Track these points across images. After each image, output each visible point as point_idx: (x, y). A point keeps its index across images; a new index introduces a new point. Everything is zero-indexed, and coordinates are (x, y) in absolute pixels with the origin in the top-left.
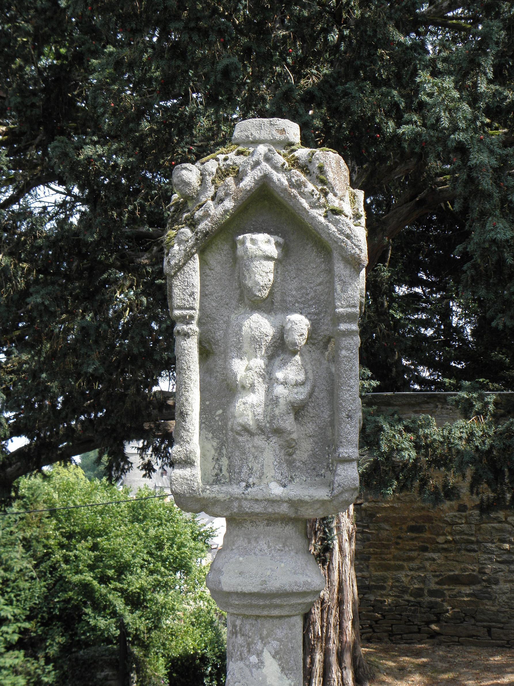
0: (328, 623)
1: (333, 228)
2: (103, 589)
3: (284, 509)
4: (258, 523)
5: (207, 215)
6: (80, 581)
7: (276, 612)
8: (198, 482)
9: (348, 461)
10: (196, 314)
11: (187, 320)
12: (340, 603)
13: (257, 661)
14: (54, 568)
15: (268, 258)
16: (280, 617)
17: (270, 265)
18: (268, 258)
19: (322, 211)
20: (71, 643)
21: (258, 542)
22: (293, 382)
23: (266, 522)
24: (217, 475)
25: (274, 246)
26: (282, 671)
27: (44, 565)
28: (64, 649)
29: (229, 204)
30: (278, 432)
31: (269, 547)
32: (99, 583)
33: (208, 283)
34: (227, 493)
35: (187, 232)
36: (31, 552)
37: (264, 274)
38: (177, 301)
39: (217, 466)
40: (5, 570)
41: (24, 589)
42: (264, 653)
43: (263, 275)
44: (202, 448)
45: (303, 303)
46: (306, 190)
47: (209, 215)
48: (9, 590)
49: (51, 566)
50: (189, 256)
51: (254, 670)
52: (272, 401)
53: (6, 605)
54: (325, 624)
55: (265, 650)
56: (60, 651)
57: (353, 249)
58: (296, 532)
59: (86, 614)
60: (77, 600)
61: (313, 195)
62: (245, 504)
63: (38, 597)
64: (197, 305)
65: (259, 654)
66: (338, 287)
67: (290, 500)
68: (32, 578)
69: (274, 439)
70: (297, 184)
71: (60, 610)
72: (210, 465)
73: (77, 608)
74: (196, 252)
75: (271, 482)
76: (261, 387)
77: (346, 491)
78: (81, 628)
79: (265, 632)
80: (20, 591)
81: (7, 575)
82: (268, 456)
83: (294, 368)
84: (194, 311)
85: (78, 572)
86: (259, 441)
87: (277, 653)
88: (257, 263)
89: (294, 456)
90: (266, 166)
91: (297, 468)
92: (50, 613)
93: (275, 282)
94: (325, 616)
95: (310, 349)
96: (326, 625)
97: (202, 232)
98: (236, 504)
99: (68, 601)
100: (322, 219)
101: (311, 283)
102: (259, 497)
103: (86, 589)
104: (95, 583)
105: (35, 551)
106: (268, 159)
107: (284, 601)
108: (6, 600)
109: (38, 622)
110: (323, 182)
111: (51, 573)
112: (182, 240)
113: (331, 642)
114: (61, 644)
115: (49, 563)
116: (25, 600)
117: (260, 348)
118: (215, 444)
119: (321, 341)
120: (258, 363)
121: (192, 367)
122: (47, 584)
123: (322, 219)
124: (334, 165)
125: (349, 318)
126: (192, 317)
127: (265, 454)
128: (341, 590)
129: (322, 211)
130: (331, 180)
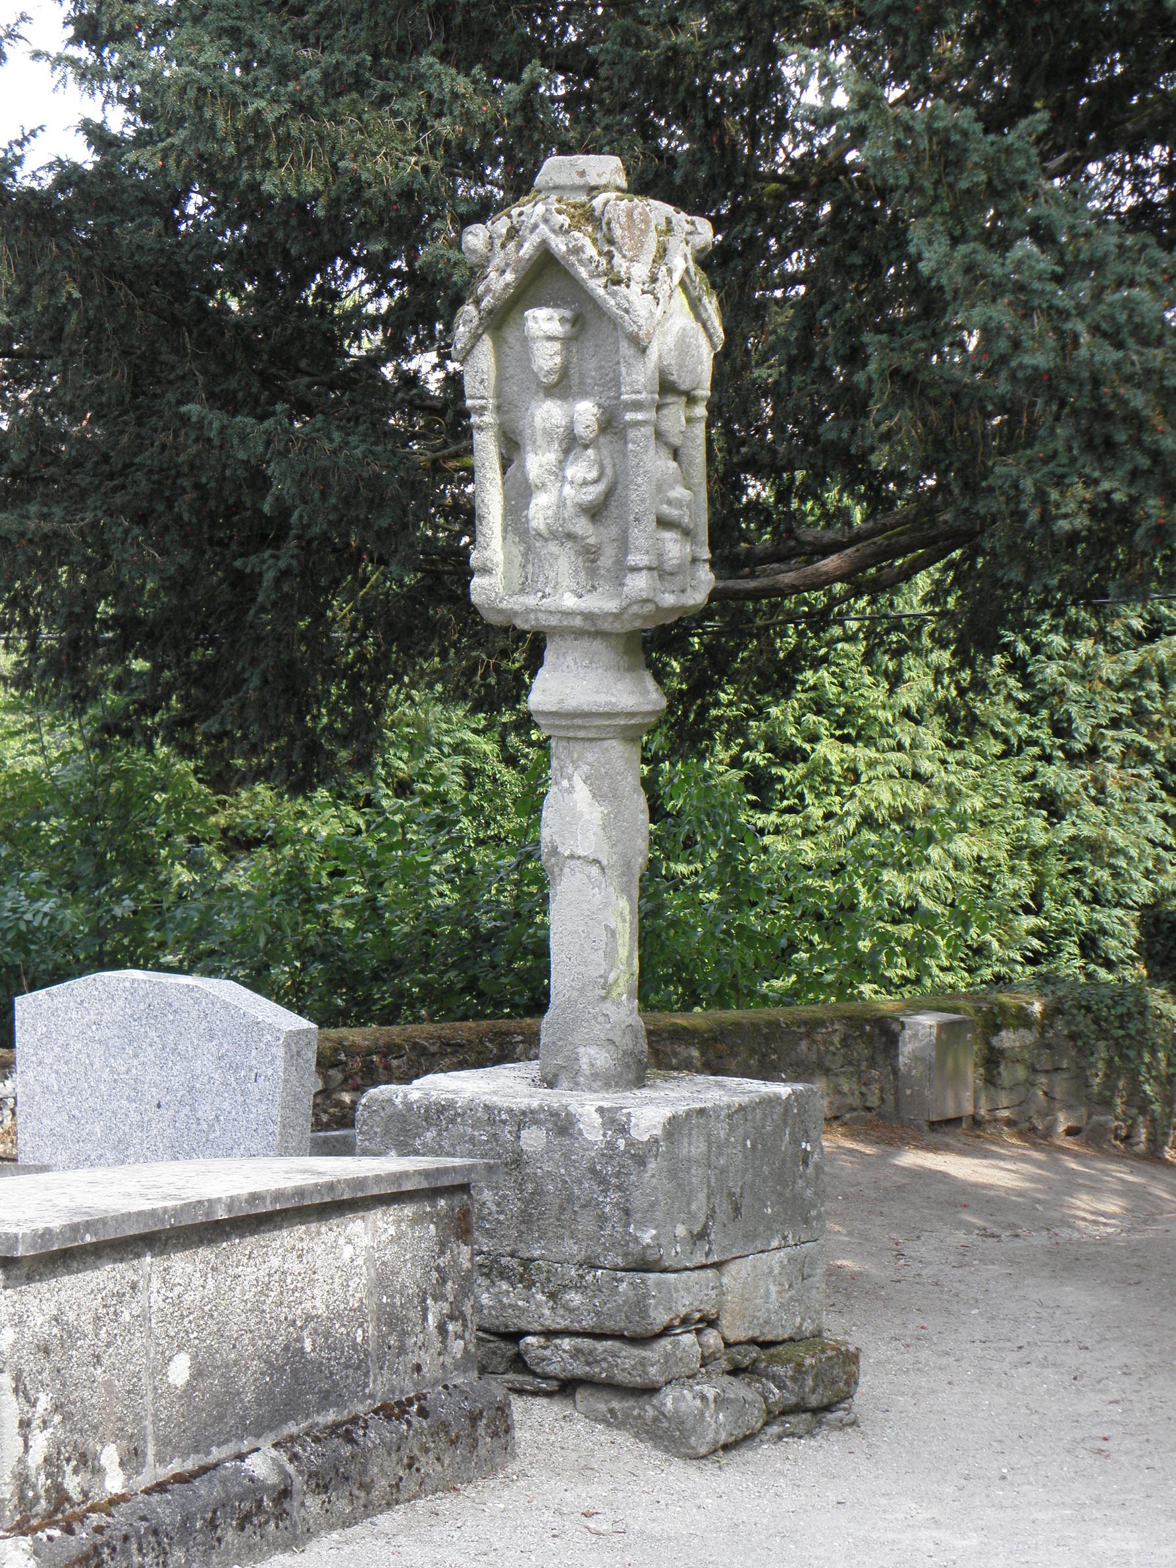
3: (578, 622)
7: (582, 734)
8: (500, 588)
9: (635, 569)
11: (481, 410)
17: (557, 346)
29: (509, 277)
30: (570, 536)
34: (523, 604)
38: (468, 391)
43: (547, 357)
45: (603, 385)
50: (476, 338)
62: (540, 615)
65: (570, 779)
69: (569, 545)
72: (517, 573)
76: (559, 486)
86: (553, 547)
87: (587, 778)
88: (538, 344)
100: (601, 291)
110: (611, 242)
120: (551, 457)
123: (601, 291)
124: (623, 220)
127: (560, 561)
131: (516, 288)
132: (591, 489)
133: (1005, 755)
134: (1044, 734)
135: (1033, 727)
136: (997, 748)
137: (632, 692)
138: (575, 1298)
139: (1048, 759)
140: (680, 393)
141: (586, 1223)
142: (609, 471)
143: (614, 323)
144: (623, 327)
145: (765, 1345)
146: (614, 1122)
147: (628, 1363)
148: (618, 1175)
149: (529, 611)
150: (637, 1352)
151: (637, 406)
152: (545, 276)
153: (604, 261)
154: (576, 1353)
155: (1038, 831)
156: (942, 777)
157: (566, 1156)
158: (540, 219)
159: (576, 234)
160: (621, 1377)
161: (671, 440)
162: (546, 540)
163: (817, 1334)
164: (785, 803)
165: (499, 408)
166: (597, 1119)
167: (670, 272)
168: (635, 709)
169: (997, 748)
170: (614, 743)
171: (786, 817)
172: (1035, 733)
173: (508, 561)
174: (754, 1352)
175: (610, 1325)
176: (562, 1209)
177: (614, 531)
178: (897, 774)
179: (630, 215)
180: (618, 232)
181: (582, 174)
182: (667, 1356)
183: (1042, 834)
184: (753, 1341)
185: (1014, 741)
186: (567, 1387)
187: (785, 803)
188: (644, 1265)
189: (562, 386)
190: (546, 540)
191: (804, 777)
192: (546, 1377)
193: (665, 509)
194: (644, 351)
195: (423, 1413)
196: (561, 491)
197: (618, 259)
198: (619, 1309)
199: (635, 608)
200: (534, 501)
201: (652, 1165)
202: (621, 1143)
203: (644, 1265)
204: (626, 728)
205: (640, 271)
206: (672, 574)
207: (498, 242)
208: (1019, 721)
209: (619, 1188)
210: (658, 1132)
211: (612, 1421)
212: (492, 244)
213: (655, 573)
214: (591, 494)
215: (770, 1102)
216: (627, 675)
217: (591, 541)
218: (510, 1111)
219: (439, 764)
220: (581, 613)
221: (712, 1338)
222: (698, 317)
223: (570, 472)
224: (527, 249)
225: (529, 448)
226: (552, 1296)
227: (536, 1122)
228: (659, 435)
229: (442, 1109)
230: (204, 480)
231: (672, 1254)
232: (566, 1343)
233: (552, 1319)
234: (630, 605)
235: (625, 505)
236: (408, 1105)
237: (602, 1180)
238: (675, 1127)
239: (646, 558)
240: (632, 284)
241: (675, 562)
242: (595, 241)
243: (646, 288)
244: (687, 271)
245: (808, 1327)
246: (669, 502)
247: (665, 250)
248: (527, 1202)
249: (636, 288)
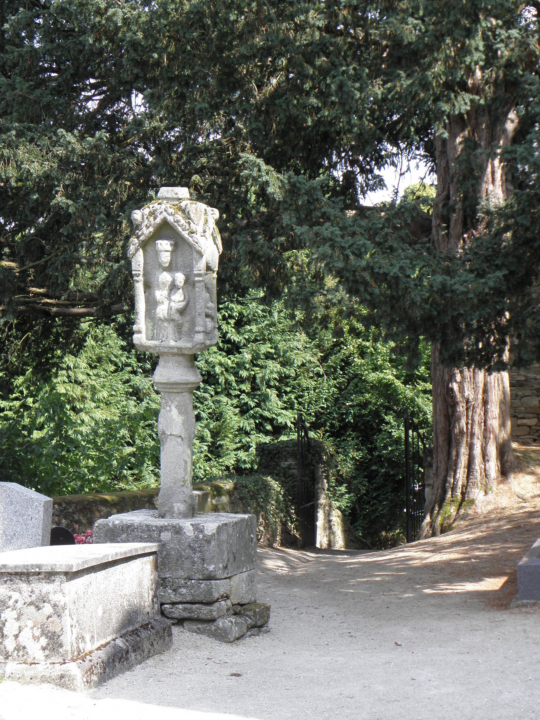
0: (473, 420)
1: (190, 239)
2: (407, 391)
3: (176, 351)
5: (143, 234)
6: (380, 381)
7: (175, 391)
9: (199, 332)
10: (141, 273)
11: (138, 275)
12: (485, 402)
14: (347, 362)
17: (169, 253)
20: (370, 460)
27: (333, 357)
28: (361, 466)
29: (151, 229)
30: (173, 320)
32: (405, 383)
35: (136, 241)
36: (316, 341)
38: (133, 268)
40: (283, 364)
41: (307, 389)
43: (166, 258)
44: (147, 326)
48: (288, 389)
49: (342, 360)
50: (137, 250)
52: (170, 308)
53: (285, 408)
54: (470, 422)
56: (356, 469)
59: (387, 423)
60: (375, 404)
63: (326, 400)
64: (142, 269)
68: (318, 375)
71: (354, 416)
72: (150, 332)
73: (376, 414)
76: (168, 303)
78: (380, 441)
80: (303, 391)
81: (285, 371)
82: (169, 329)
85: (376, 368)
90: (165, 214)
92: (342, 420)
93: (171, 261)
94: (470, 414)
96: (471, 423)
99: (364, 405)
103: (385, 389)
104: (398, 383)
105: (321, 340)
106: (166, 211)
108: (285, 402)
109: (326, 431)
110: (189, 219)
111: (342, 369)
113: (475, 437)
114: (356, 460)
115: (340, 356)
116: (310, 403)
119: (189, 282)
120: (165, 292)
122: (338, 383)
128: (485, 391)
133: (116, 371)
134: (133, 361)
135: (128, 358)
136: (113, 368)
138: (184, 591)
139: (134, 372)
141: (187, 564)
143: (190, 246)
145: (242, 605)
146: (197, 528)
147: (205, 612)
148: (199, 547)
149: (156, 346)
150: (208, 607)
151: (199, 275)
152: (165, 230)
154: (185, 609)
155: (132, 407)
156: (88, 382)
157: (179, 541)
160: (202, 616)
163: (255, 602)
164: (14, 395)
165: (144, 275)
166: (191, 528)
169: (113, 368)
171: (15, 402)
172: (129, 361)
173: (147, 329)
174: (239, 608)
175: (198, 599)
176: (178, 560)
177: (188, 318)
178: (67, 381)
179: (196, 209)
180: (192, 215)
181: (176, 194)
182: (218, 608)
183: (133, 408)
184: (239, 604)
185: (120, 365)
186: (180, 622)
187: (14, 395)
188: (210, 578)
191: (23, 383)
192: (172, 618)
195: (152, 628)
197: (192, 224)
198: (201, 593)
201: (213, 543)
202: (201, 536)
203: (210, 578)
205: (200, 229)
208: (122, 355)
209: (200, 552)
210: (215, 531)
211: (199, 632)
214: (181, 305)
215: (243, 520)
218: (156, 526)
221: (229, 602)
223: (173, 298)
224: (158, 220)
226: (175, 590)
227: (167, 530)
229: (128, 527)
231: (219, 574)
232: (180, 606)
233: (174, 598)
236: (115, 526)
237: (194, 550)
238: (219, 529)
245: (253, 599)
248: (163, 558)
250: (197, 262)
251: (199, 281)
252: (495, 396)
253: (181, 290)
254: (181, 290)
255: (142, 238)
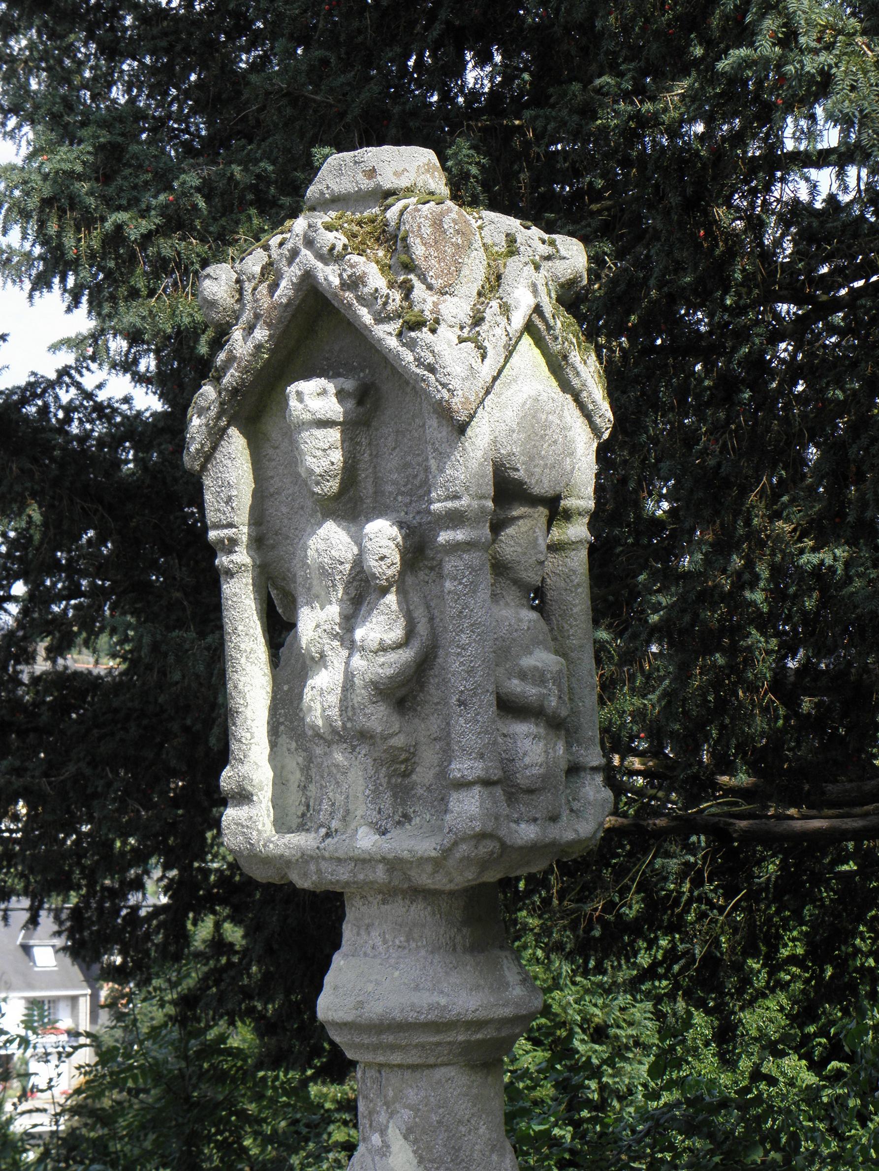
1: (408, 356)
3: (380, 874)
4: (370, 899)
7: (396, 1058)
9: (463, 785)
10: (243, 533)
13: (380, 1144)
15: (324, 424)
16: (413, 1068)
17: (334, 435)
18: (324, 424)
19: (394, 326)
21: (369, 933)
22: (375, 646)
23: (380, 897)
24: (303, 815)
25: (335, 400)
26: (420, 1162)
29: (261, 334)
30: (364, 736)
31: (385, 942)
33: (271, 474)
37: (319, 453)
38: (211, 516)
39: (303, 800)
42: (390, 1131)
43: (322, 454)
46: (366, 290)
47: (235, 357)
50: (217, 436)
51: (377, 1158)
55: (391, 1125)
57: (438, 391)
58: (434, 914)
61: (376, 298)
62: (324, 865)
65: (383, 1132)
66: (433, 463)
67: (384, 858)
70: (353, 282)
74: (228, 425)
75: (361, 826)
76: (349, 654)
77: (463, 839)
79: (391, 1094)
82: (352, 777)
83: (382, 618)
84: (234, 530)
88: (305, 435)
89: (414, 777)
90: (306, 255)
91: (419, 798)
95: (427, 578)
97: (226, 389)
98: (313, 867)
101: (418, 455)
102: (340, 854)
106: (309, 243)
107: (402, 1039)
110: (409, 267)
112: (202, 408)
117: (334, 586)
118: (300, 760)
119: (418, 551)
121: (240, 628)
123: (392, 343)
124: (427, 230)
125: (452, 520)
126: (233, 542)
129: (394, 326)
130: (421, 262)
131: (272, 352)
132: (392, 657)
137: (478, 987)
140: (534, 501)
142: (422, 628)
144: (428, 395)
149: (306, 858)
151: (455, 519)
152: (315, 329)
153: (397, 296)
158: (310, 245)
159: (354, 258)
161: (524, 575)
162: (329, 744)
165: (258, 543)
167: (506, 310)
168: (482, 1015)
170: (450, 1072)
173: (280, 782)
180: (419, 250)
189: (349, 502)
190: (329, 744)
193: (516, 686)
194: (462, 429)
196: (347, 664)
197: (419, 291)
199: (464, 849)
200: (310, 682)
204: (467, 1048)
205: (457, 308)
206: (530, 791)
207: (248, 287)
212: (241, 291)
213: (498, 791)
216: (468, 957)
217: (398, 741)
219: (633, 1010)
220: (383, 860)
222: (565, 386)
225: (301, 600)
228: (500, 568)
230: (189, 722)
234: (455, 844)
235: (446, 682)
239: (479, 765)
240: (442, 329)
241: (535, 771)
242: (385, 269)
243: (465, 333)
244: (538, 309)
246: (523, 676)
247: (499, 277)
249: (447, 336)
250: (443, 457)
251: (455, 548)
252: (37, 1118)
253: (391, 598)
254: (391, 598)
255: (231, 377)
